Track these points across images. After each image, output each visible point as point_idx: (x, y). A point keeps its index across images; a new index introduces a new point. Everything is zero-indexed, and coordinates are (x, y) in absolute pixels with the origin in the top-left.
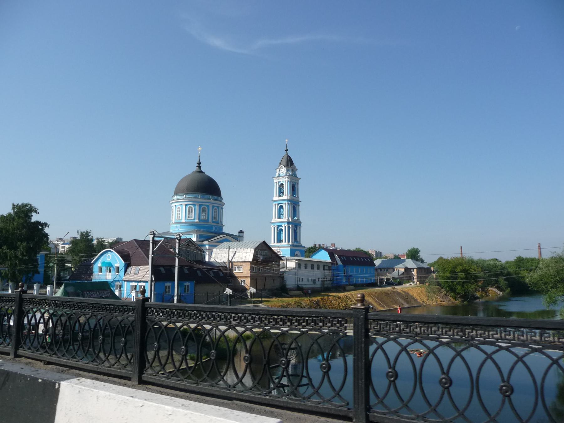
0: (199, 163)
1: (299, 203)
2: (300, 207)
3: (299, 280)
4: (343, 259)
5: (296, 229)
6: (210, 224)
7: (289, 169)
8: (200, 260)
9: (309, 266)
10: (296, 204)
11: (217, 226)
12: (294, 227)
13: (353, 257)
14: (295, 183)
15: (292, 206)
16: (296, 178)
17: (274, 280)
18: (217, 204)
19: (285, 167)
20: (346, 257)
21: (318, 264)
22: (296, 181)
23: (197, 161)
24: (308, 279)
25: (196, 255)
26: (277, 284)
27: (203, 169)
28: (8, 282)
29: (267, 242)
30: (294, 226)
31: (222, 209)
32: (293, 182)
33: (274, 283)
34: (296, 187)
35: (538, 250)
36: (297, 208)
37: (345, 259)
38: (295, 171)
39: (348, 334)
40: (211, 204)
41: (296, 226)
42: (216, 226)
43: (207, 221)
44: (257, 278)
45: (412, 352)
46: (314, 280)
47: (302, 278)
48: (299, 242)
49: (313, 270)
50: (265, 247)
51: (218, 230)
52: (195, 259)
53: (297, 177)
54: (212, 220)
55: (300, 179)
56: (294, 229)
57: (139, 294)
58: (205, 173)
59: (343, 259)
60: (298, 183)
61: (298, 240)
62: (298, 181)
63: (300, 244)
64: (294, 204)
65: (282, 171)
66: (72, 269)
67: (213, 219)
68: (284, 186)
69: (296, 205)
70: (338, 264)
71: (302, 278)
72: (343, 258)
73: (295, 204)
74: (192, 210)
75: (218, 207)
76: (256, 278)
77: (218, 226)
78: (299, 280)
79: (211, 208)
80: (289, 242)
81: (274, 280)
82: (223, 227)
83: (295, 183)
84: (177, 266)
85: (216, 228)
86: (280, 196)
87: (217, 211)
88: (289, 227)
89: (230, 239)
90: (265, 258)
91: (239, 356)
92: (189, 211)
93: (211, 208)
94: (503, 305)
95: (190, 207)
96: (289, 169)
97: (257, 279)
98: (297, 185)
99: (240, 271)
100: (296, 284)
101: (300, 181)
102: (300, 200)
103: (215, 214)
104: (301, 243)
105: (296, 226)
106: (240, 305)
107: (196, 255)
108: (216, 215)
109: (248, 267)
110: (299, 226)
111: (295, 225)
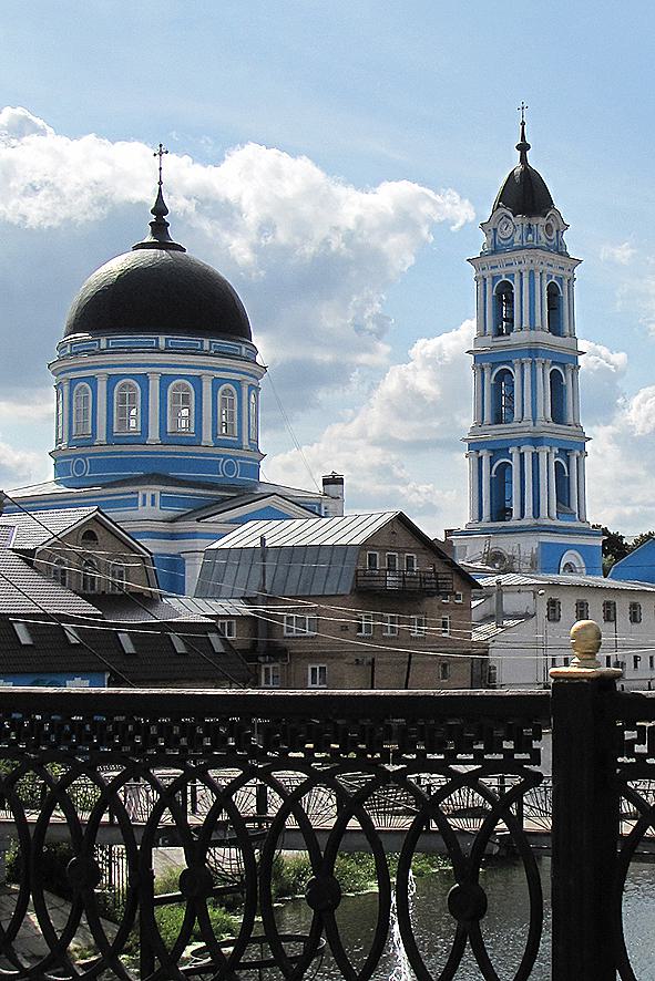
6: (149, 449)
10: (563, 365)
11: (84, 456)
14: (560, 280)
16: (564, 259)
17: (444, 666)
27: (174, 236)
31: (255, 388)
32: (550, 277)
33: (444, 678)
34: (564, 294)
35: (463, 464)
36: (567, 380)
40: (208, 372)
41: (565, 453)
42: (231, 457)
43: (195, 441)
50: (404, 539)
51: (237, 476)
52: (93, 588)
54: (215, 434)
57: (548, 823)
58: (184, 250)
64: (554, 363)
66: (362, 744)
68: (516, 291)
69: (564, 369)
76: (370, 659)
77: (242, 458)
79: (154, 385)
80: (536, 514)
81: (444, 666)
83: (560, 280)
85: (230, 467)
86: (499, 333)
88: (535, 457)
89: (282, 510)
90: (404, 581)
93: (154, 385)
105: (565, 453)
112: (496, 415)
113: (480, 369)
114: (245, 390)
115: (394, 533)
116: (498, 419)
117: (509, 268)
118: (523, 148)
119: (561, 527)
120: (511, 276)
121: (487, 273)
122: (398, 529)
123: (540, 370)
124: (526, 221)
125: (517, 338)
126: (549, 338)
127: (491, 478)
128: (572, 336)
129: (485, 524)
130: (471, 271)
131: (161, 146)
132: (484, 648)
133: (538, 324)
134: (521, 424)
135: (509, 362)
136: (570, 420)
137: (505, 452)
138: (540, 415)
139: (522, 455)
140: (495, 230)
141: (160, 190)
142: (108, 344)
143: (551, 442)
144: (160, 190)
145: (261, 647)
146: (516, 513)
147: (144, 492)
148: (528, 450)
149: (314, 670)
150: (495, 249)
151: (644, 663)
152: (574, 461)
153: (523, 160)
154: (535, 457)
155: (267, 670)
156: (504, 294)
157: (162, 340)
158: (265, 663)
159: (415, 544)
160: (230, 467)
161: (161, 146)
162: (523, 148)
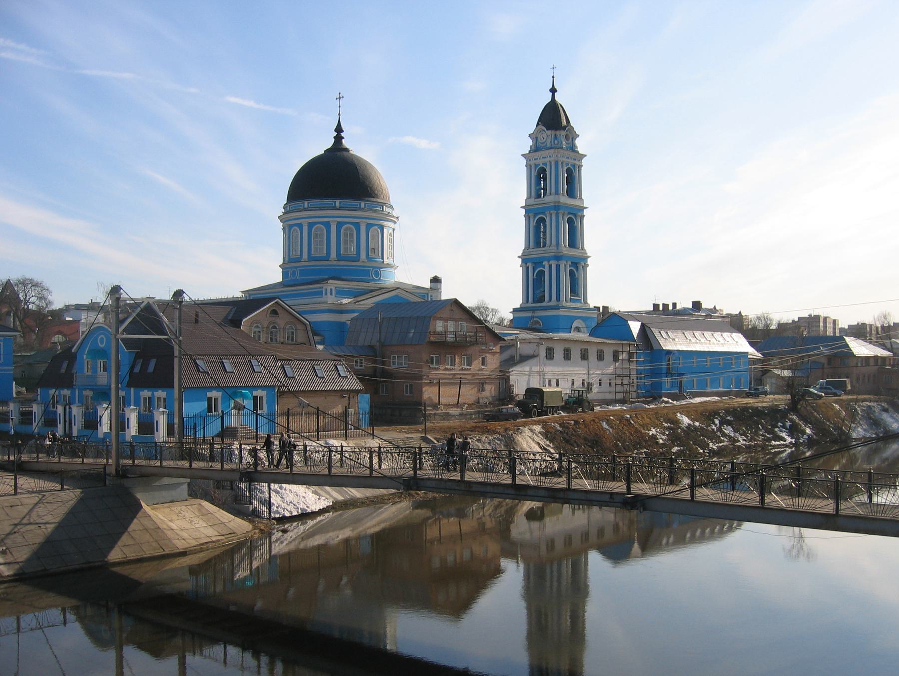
0: (339, 130)
1: (583, 210)
2: (585, 220)
5: (575, 270)
9: (576, 354)
11: (296, 267)
12: (570, 266)
21: (567, 346)
22: (569, 160)
24: (600, 380)
25: (292, 333)
28: (667, 435)
29: (463, 303)
30: (570, 263)
38: (573, 139)
39: (45, 455)
40: (364, 220)
43: (327, 258)
45: (274, 498)
46: (588, 384)
49: (586, 362)
53: (578, 152)
55: (586, 156)
60: (580, 167)
62: (581, 160)
64: (569, 213)
69: (576, 217)
70: (654, 349)
73: (572, 214)
74: (351, 235)
79: (333, 228)
84: (176, 357)
95: (346, 229)
101: (584, 161)
102: (585, 206)
107: (292, 333)
111: (572, 262)
115: (452, 310)
118: (553, 91)
121: (532, 163)
123: (561, 218)
127: (534, 279)
129: (530, 305)
131: (340, 94)
135: (544, 213)
148: (554, 263)
154: (558, 267)
157: (338, 202)
161: (340, 94)
162: (553, 91)
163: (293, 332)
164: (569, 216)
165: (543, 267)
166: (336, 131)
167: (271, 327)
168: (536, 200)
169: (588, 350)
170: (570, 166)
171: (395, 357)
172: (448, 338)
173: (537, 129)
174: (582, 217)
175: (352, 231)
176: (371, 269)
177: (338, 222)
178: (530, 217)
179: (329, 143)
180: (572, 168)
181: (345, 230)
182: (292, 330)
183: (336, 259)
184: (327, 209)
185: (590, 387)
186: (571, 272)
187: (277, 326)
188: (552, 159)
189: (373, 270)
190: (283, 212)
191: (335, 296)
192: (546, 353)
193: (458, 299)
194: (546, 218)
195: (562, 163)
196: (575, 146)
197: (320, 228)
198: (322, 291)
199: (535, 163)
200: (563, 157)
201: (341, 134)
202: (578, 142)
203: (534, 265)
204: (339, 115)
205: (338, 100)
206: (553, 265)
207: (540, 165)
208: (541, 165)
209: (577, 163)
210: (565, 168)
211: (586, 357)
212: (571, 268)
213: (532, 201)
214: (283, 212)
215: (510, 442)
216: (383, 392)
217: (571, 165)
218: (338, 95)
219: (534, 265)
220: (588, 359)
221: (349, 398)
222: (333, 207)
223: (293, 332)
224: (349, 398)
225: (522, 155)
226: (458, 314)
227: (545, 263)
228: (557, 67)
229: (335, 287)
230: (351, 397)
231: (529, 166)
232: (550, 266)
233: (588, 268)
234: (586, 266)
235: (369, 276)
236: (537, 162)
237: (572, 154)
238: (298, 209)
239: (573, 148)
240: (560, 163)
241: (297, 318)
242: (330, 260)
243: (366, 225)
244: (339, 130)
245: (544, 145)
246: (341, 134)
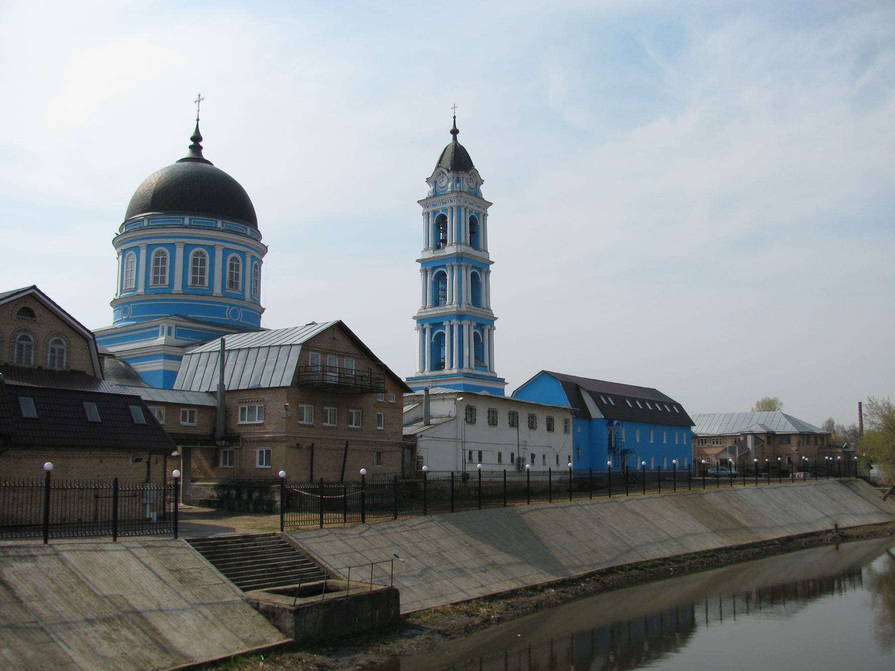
0: (197, 138)
3: (470, 458)
4: (605, 403)
7: (461, 176)
8: (84, 369)
10: (480, 269)
11: (239, 307)
12: (475, 328)
13: (633, 400)
14: (478, 214)
15: (469, 273)
17: (379, 454)
18: (241, 245)
19: (448, 171)
20: (614, 397)
21: (493, 406)
23: (192, 133)
26: (391, 467)
27: (205, 154)
30: (474, 324)
32: (471, 211)
33: (378, 463)
34: (480, 223)
36: (482, 279)
37: (613, 404)
41: (480, 326)
44: (313, 445)
46: (519, 458)
47: (480, 453)
48: (490, 368)
52: (61, 365)
56: (475, 334)
58: (212, 165)
59: (605, 403)
60: (485, 215)
61: (487, 363)
62: (485, 209)
63: (493, 372)
64: (473, 267)
65: (444, 184)
67: (227, 286)
69: (480, 272)
71: (480, 453)
72: (607, 401)
75: (243, 254)
76: (310, 445)
77: (243, 307)
78: (470, 458)
79: (219, 254)
80: (461, 365)
81: (379, 454)
82: (261, 314)
83: (478, 214)
85: (235, 314)
86: (438, 247)
87: (238, 266)
88: (461, 328)
91: (864, 411)
92: (195, 262)
93: (219, 254)
94: (155, 545)
95: (159, 253)
96: (461, 176)
97: (312, 448)
98: (481, 220)
99: (257, 422)
100: (460, 469)
101: (490, 210)
103: (231, 274)
104: (496, 370)
105: (480, 326)
106: (39, 538)
108: (237, 275)
109: (279, 406)
110: (488, 327)
112: (436, 301)
113: (425, 272)
114: (249, 260)
115: (334, 338)
116: (436, 303)
117: (444, 206)
118: (455, 132)
119: (476, 375)
120: (446, 210)
121: (431, 209)
122: (339, 336)
123: (464, 272)
124: (456, 175)
125: (450, 250)
126: (470, 250)
127: (431, 343)
128: (486, 251)
129: (427, 373)
130: (420, 209)
131: (199, 95)
132: (413, 437)
133: (463, 240)
134: (451, 305)
135: (444, 266)
136: (484, 305)
137: (440, 325)
138: (464, 300)
139: (452, 327)
140: (436, 182)
141: (198, 123)
142: (149, 223)
143: (471, 318)
144: (198, 123)
145: (218, 434)
146: (447, 366)
147: (163, 325)
149: (261, 452)
150: (435, 194)
151: (538, 460)
152: (486, 332)
153: (455, 139)
154: (461, 328)
155: (225, 453)
156: (441, 223)
157: (187, 221)
158: (225, 446)
159: (353, 350)
160: (235, 314)
161: (199, 95)
162: (455, 132)
163: (63, 350)
164: (472, 271)
165: (443, 329)
166: (192, 139)
167: (19, 337)
168: (435, 252)
169: (517, 413)
170: (473, 214)
171: (245, 408)
172: (328, 378)
173: (437, 171)
174: (488, 272)
175: (204, 256)
176: (228, 307)
177: (186, 244)
178: (427, 272)
179: (187, 153)
180: (476, 217)
181: (195, 255)
182: (61, 347)
183: (182, 292)
184: (173, 227)
185: (521, 463)
186: (476, 334)
187: (30, 336)
188: (454, 204)
189: (231, 309)
190: (117, 234)
191: (176, 338)
192: (466, 414)
193: (342, 321)
194: (446, 273)
195: (465, 209)
196: (479, 192)
197: (163, 252)
198: (158, 331)
199: (433, 210)
200: (466, 202)
201: (200, 143)
202: (482, 188)
203: (432, 327)
204: (198, 120)
205: (197, 103)
206: (454, 326)
207: (439, 211)
208: (441, 212)
209: (483, 211)
210: (468, 217)
211: (515, 422)
212: (475, 331)
213: (429, 255)
214: (117, 234)
215: (83, 522)
216: (225, 463)
217: (475, 213)
218: (198, 97)
219: (432, 327)
220: (518, 426)
221: (148, 463)
222: (180, 225)
223: (63, 350)
224: (148, 463)
225: (419, 202)
226: (344, 345)
227: (446, 323)
228: (459, 106)
229: (176, 326)
230: (153, 461)
231: (427, 215)
232: (452, 327)
233: (495, 331)
234: (492, 328)
235: (226, 317)
236: (436, 208)
237: (476, 200)
238: (135, 229)
239: (477, 195)
240: (463, 209)
241: (70, 327)
242: (173, 292)
243: (223, 249)
244: (197, 138)
245: (444, 189)
246: (200, 143)
